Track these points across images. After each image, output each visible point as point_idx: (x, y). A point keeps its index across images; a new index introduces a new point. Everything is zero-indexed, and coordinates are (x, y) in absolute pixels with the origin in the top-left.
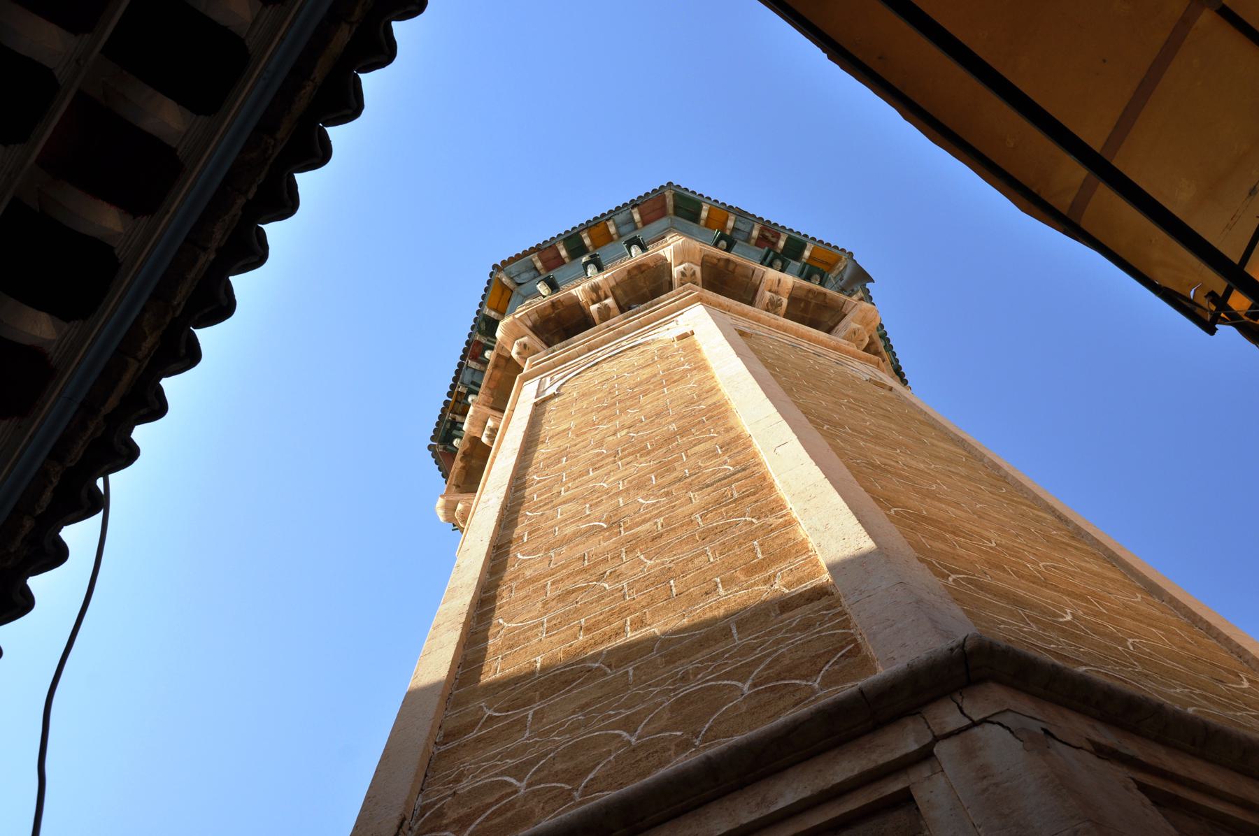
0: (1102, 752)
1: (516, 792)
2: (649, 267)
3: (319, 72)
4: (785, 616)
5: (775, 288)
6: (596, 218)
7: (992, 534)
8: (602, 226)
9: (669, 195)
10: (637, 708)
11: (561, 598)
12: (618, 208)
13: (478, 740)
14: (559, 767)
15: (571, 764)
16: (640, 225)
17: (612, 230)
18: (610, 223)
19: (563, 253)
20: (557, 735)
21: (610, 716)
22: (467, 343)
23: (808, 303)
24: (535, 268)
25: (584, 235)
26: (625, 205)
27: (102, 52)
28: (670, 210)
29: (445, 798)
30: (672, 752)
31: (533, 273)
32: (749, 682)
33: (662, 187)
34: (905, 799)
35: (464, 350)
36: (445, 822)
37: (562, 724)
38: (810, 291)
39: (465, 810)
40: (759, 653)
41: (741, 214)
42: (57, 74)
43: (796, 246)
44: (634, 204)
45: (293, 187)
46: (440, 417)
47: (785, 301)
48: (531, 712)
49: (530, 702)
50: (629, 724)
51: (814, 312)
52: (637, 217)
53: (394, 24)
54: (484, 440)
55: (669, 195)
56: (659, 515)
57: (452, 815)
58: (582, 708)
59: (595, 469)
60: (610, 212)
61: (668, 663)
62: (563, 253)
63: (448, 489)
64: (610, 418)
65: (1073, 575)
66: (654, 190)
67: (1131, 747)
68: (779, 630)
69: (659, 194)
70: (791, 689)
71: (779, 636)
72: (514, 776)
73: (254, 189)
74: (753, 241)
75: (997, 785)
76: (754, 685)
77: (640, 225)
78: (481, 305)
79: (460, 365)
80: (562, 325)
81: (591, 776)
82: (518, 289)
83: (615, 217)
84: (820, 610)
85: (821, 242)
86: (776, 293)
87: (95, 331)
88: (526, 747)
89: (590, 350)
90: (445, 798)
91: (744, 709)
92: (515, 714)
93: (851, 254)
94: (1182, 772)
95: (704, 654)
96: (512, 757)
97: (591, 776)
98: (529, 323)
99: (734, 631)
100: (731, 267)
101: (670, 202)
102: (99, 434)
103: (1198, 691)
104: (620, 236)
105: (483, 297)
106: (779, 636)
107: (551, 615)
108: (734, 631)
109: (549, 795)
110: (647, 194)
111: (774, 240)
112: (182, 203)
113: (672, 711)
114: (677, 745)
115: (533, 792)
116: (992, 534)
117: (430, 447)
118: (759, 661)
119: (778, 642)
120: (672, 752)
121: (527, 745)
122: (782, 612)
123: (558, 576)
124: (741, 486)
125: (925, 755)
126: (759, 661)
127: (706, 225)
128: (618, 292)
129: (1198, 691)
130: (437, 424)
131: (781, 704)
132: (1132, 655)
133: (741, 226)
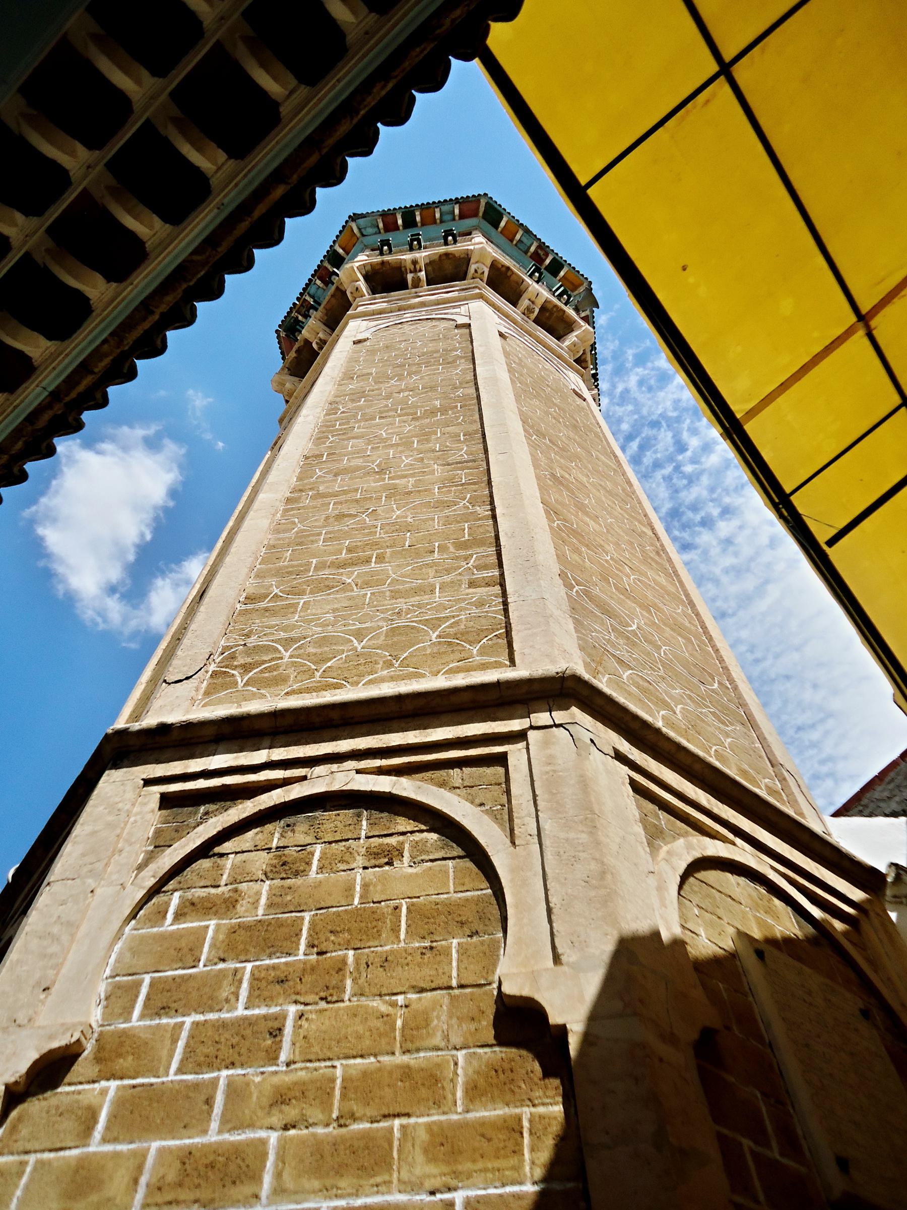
0: (620, 757)
1: (281, 658)
2: (454, 256)
3: (260, 210)
4: (471, 590)
5: (533, 299)
6: (428, 203)
7: (611, 548)
8: (431, 210)
9: (483, 202)
10: (367, 625)
11: (340, 517)
12: (445, 201)
13: (266, 610)
14: (312, 650)
15: (319, 651)
16: (457, 218)
17: (438, 215)
18: (437, 210)
19: (400, 222)
20: (314, 626)
21: (349, 624)
22: (318, 266)
24: (378, 226)
25: (417, 213)
26: (451, 200)
27: (106, 165)
28: (481, 214)
29: (239, 645)
30: (380, 666)
31: (376, 230)
32: (437, 633)
33: (479, 195)
34: (501, 760)
35: (315, 271)
36: (235, 663)
37: (319, 619)
38: (556, 306)
39: (249, 660)
40: (447, 613)
41: (527, 231)
42: (71, 174)
43: (557, 266)
44: (457, 201)
45: (223, 282)
46: (288, 313)
47: (537, 311)
48: (302, 601)
49: (302, 593)
50: (359, 634)
51: (553, 323)
52: (457, 211)
53: (318, 190)
54: (315, 346)
55: (483, 202)
56: (412, 475)
57: (240, 660)
58: (334, 610)
59: (381, 418)
60: (439, 202)
61: (393, 597)
62: (400, 222)
63: (282, 369)
64: (401, 377)
65: (647, 586)
66: (474, 196)
67: (635, 755)
68: (465, 600)
69: (477, 198)
70: (461, 648)
71: (463, 605)
72: (283, 646)
73: (195, 280)
74: (529, 254)
75: (554, 771)
76: (439, 636)
77: (457, 218)
78: (334, 242)
79: (310, 280)
80: (387, 280)
81: (329, 664)
82: (362, 239)
83: (442, 208)
84: (491, 595)
85: (574, 268)
86: (533, 302)
87: (69, 350)
88: (294, 627)
89: (399, 310)
90: (239, 645)
91: (429, 651)
92: (292, 600)
93: (590, 283)
94: (656, 773)
95: (415, 600)
96: (285, 631)
97: (329, 664)
98: (364, 272)
99: (437, 590)
100: (509, 273)
101: (482, 209)
102: (60, 412)
103: (688, 692)
104: (442, 221)
105: (337, 237)
106: (463, 605)
107: (330, 529)
108: (437, 590)
109: (302, 669)
110: (468, 197)
111: (544, 257)
112: (143, 282)
113: (386, 636)
114: (384, 662)
115: (292, 662)
116: (611, 548)
117: (277, 331)
118: (447, 618)
119: (461, 609)
120: (380, 666)
121: (295, 625)
122: (470, 587)
123: (342, 498)
124: (471, 474)
125: (520, 736)
126: (447, 618)
127: (501, 232)
128: (430, 268)
129: (688, 692)
130: (285, 317)
131: (452, 656)
132: (661, 661)
133: (524, 240)
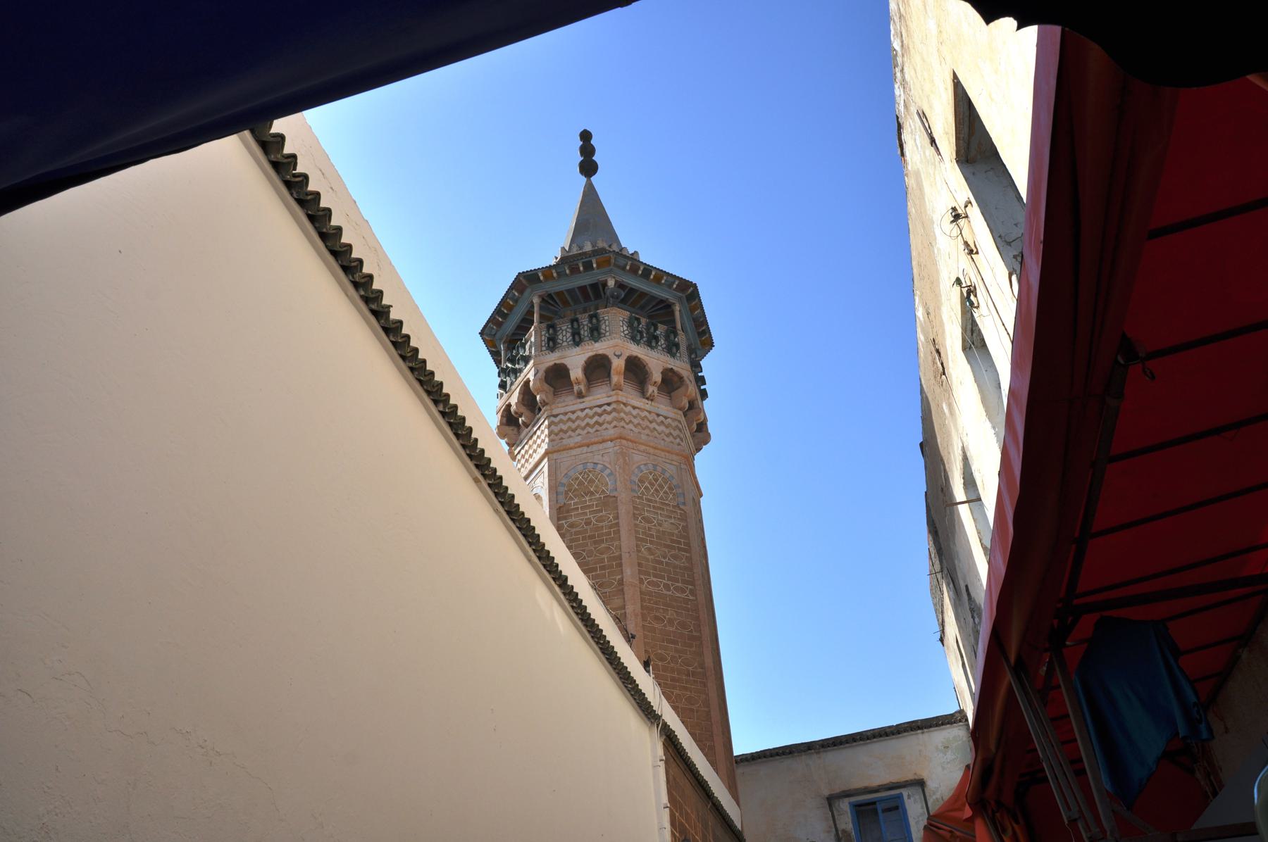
101: (524, 281)
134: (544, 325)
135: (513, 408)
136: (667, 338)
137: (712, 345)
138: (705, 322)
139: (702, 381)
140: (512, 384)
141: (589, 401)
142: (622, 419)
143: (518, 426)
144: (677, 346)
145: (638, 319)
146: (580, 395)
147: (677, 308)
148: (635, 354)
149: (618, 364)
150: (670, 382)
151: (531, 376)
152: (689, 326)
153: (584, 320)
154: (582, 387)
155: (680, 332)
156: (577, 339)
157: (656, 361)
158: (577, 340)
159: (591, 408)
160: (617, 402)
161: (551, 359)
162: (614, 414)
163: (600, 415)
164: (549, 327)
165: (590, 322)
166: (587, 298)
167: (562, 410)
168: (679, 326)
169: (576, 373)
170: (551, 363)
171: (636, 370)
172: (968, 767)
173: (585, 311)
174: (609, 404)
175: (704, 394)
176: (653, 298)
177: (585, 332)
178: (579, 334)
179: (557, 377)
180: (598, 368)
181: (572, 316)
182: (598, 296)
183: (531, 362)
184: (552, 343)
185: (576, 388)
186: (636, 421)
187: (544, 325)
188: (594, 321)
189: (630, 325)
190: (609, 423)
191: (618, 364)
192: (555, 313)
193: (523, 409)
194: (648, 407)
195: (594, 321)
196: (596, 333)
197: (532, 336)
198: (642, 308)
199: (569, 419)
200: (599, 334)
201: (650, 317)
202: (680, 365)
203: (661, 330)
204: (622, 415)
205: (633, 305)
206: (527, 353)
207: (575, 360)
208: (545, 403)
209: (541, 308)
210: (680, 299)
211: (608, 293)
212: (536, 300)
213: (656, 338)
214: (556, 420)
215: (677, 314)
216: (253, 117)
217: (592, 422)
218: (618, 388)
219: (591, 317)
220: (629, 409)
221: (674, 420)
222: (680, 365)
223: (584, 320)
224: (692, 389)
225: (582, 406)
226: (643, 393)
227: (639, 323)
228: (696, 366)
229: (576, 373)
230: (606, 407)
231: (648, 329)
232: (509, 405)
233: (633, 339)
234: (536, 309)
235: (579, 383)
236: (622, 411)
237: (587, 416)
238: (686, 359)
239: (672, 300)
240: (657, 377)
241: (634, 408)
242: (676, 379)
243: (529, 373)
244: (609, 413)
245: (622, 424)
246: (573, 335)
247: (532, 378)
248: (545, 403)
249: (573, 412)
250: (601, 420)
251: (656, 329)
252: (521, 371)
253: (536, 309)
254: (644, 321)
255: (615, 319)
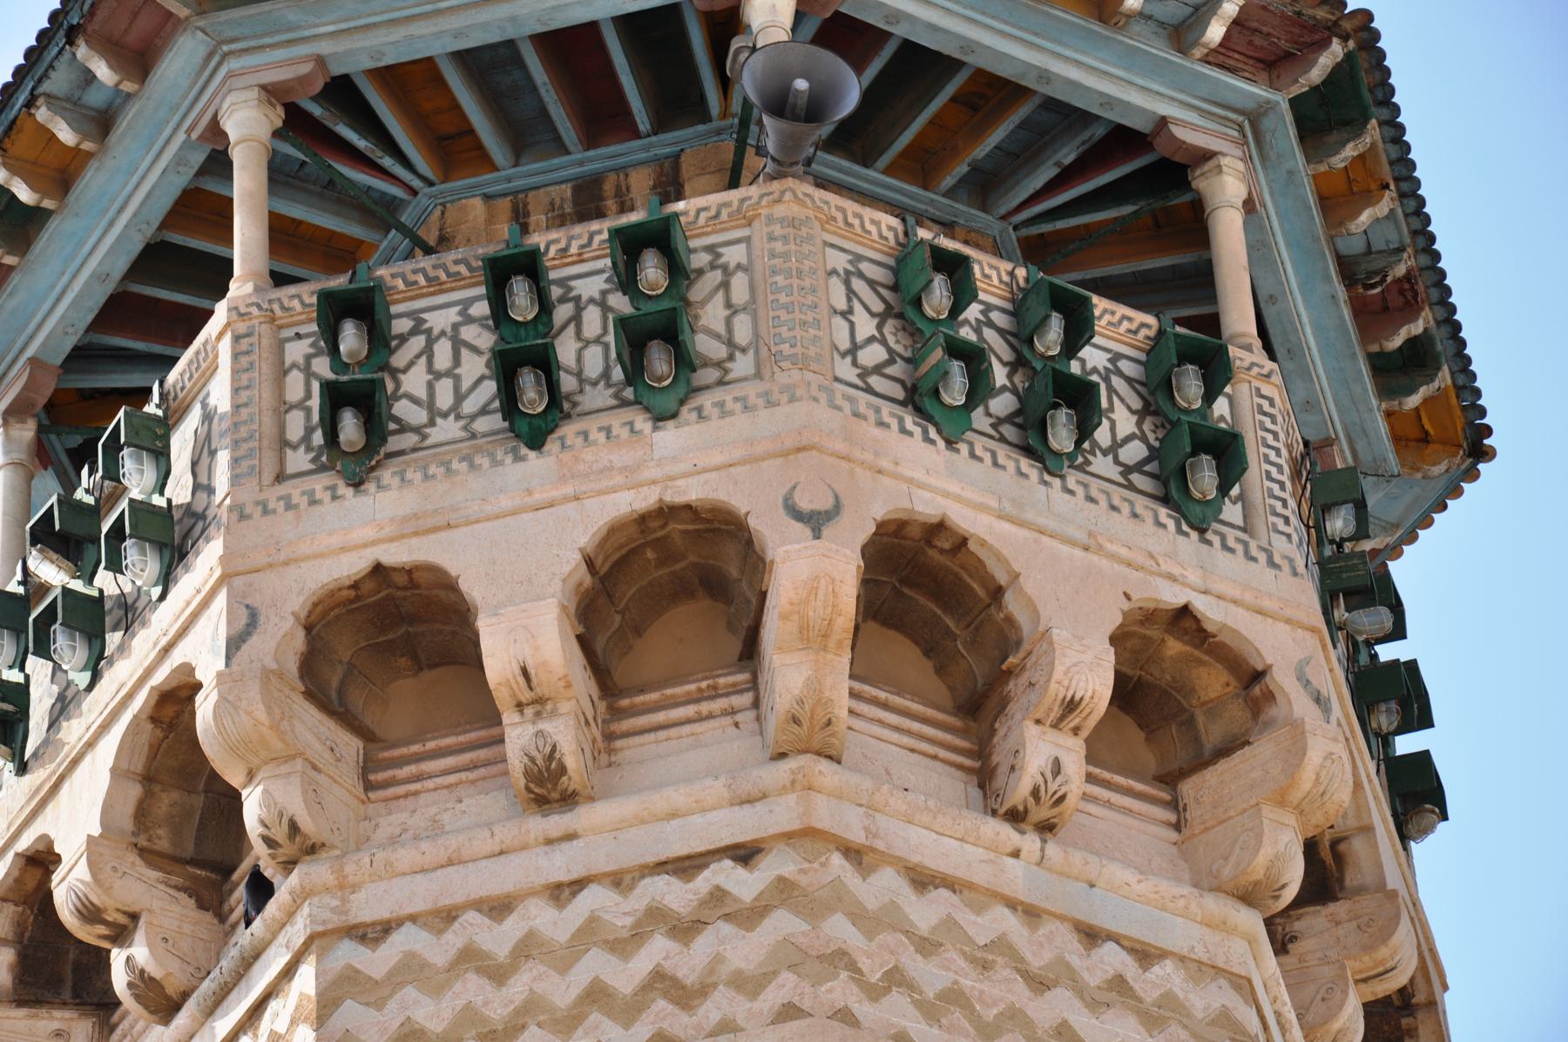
5: (526, 696)
23: (660, 544)
83: (46, 87)
134: (302, 298)
135: (69, 887)
136: (1156, 393)
137: (1477, 448)
138: (1427, 285)
139: (1392, 696)
140: (64, 706)
141: (607, 829)
142: (841, 959)
143: (103, 1005)
144: (1226, 451)
145: (954, 268)
146: (548, 789)
147: (1227, 189)
148: (928, 507)
149: (812, 578)
150: (1174, 704)
151: (204, 654)
152: (1318, 314)
153: (580, 260)
154: (565, 734)
155: (1246, 355)
156: (532, 396)
157: (1078, 557)
158: (528, 394)
159: (619, 881)
160: (807, 836)
161: (353, 532)
162: (782, 923)
163: (684, 930)
164: (334, 311)
165: (627, 280)
166: (603, 117)
167: (419, 894)
168: (1239, 317)
169: (524, 637)
170: (354, 565)
171: (927, 597)
172: (1445, 987)
173: (587, 201)
174: (745, 854)
175: (1416, 794)
176: (1062, 116)
177: (585, 351)
178: (545, 363)
179: (390, 649)
180: (671, 593)
181: (500, 239)
182: (678, 102)
183: (207, 560)
184: (358, 420)
185: (519, 737)
186: (932, 975)
187: (302, 298)
188: (351, 338)
189: (902, 304)
190: (749, 985)
191: (812, 578)
192: (382, 214)
193: (142, 888)
194: (1017, 877)
195: (351, 338)
196: (659, 350)
197: (213, 371)
198: (983, 185)
199: (470, 957)
200: (685, 362)
201: (1034, 251)
202: (1253, 588)
203: (1118, 333)
204: (840, 929)
205: (920, 165)
206: (179, 490)
207: (518, 541)
208: (300, 846)
209: (280, 175)
210: (1253, 122)
211: (749, 83)
212: (247, 125)
213: (1081, 399)
214: (376, 961)
215: (1229, 234)
216: (1088, 342)
217: (626, 976)
218: (813, 740)
219: (630, 245)
220: (885, 885)
221: (1203, 970)
222: (1253, 588)
223: (580, 260)
224: (1327, 756)
225: (560, 865)
226: (984, 773)
227: (963, 292)
228: (1357, 589)
229: (524, 637)
230: (725, 874)
231: (1022, 337)
232: (42, 861)
233: (919, 399)
234: (247, 188)
235: (536, 704)
236: (839, 900)
237: (590, 933)
238: (1291, 546)
239: (1192, 130)
240: (1086, 670)
241: (922, 880)
242: (1213, 682)
243: (187, 627)
244: (750, 916)
245: (840, 991)
246: (506, 367)
247: (204, 654)
248: (300, 846)
249: (499, 908)
250: (689, 962)
251: (1078, 331)
252: (130, 613)
253: (247, 188)
254: (995, 276)
255: (795, 254)
